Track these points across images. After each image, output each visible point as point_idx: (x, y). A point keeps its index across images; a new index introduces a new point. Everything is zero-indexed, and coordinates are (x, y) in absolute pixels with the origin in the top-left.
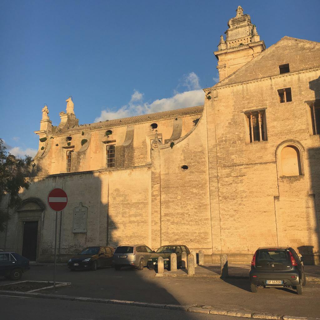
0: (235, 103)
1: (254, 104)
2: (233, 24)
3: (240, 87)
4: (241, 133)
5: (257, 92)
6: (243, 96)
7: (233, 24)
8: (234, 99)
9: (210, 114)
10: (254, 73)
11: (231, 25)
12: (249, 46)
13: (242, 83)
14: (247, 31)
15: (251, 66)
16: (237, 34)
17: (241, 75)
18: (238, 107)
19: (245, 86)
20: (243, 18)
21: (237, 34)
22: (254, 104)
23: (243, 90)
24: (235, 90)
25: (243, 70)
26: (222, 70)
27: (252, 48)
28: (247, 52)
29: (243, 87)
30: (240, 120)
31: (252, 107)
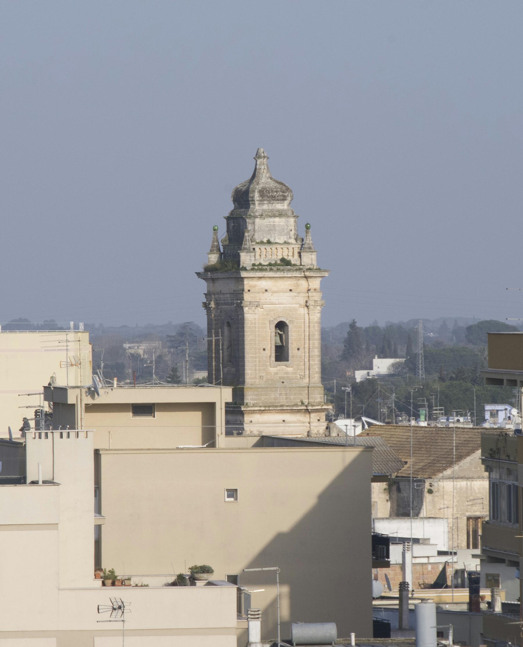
0: (458, 503)
1: (478, 507)
2: (261, 201)
3: (462, 484)
4: (463, 541)
5: (482, 494)
6: (466, 496)
7: (261, 201)
8: (457, 497)
9: (430, 512)
10: (479, 469)
11: (258, 201)
12: (305, 275)
13: (468, 478)
14: (290, 228)
15: (476, 458)
16: (271, 230)
17: (465, 467)
18: (461, 509)
19: (469, 483)
20: (281, 193)
21: (271, 230)
22: (478, 507)
23: (467, 488)
24: (459, 486)
25: (467, 462)
26: (250, 311)
27: (307, 279)
28: (296, 282)
29: (467, 484)
30: (462, 525)
31: (476, 511)
